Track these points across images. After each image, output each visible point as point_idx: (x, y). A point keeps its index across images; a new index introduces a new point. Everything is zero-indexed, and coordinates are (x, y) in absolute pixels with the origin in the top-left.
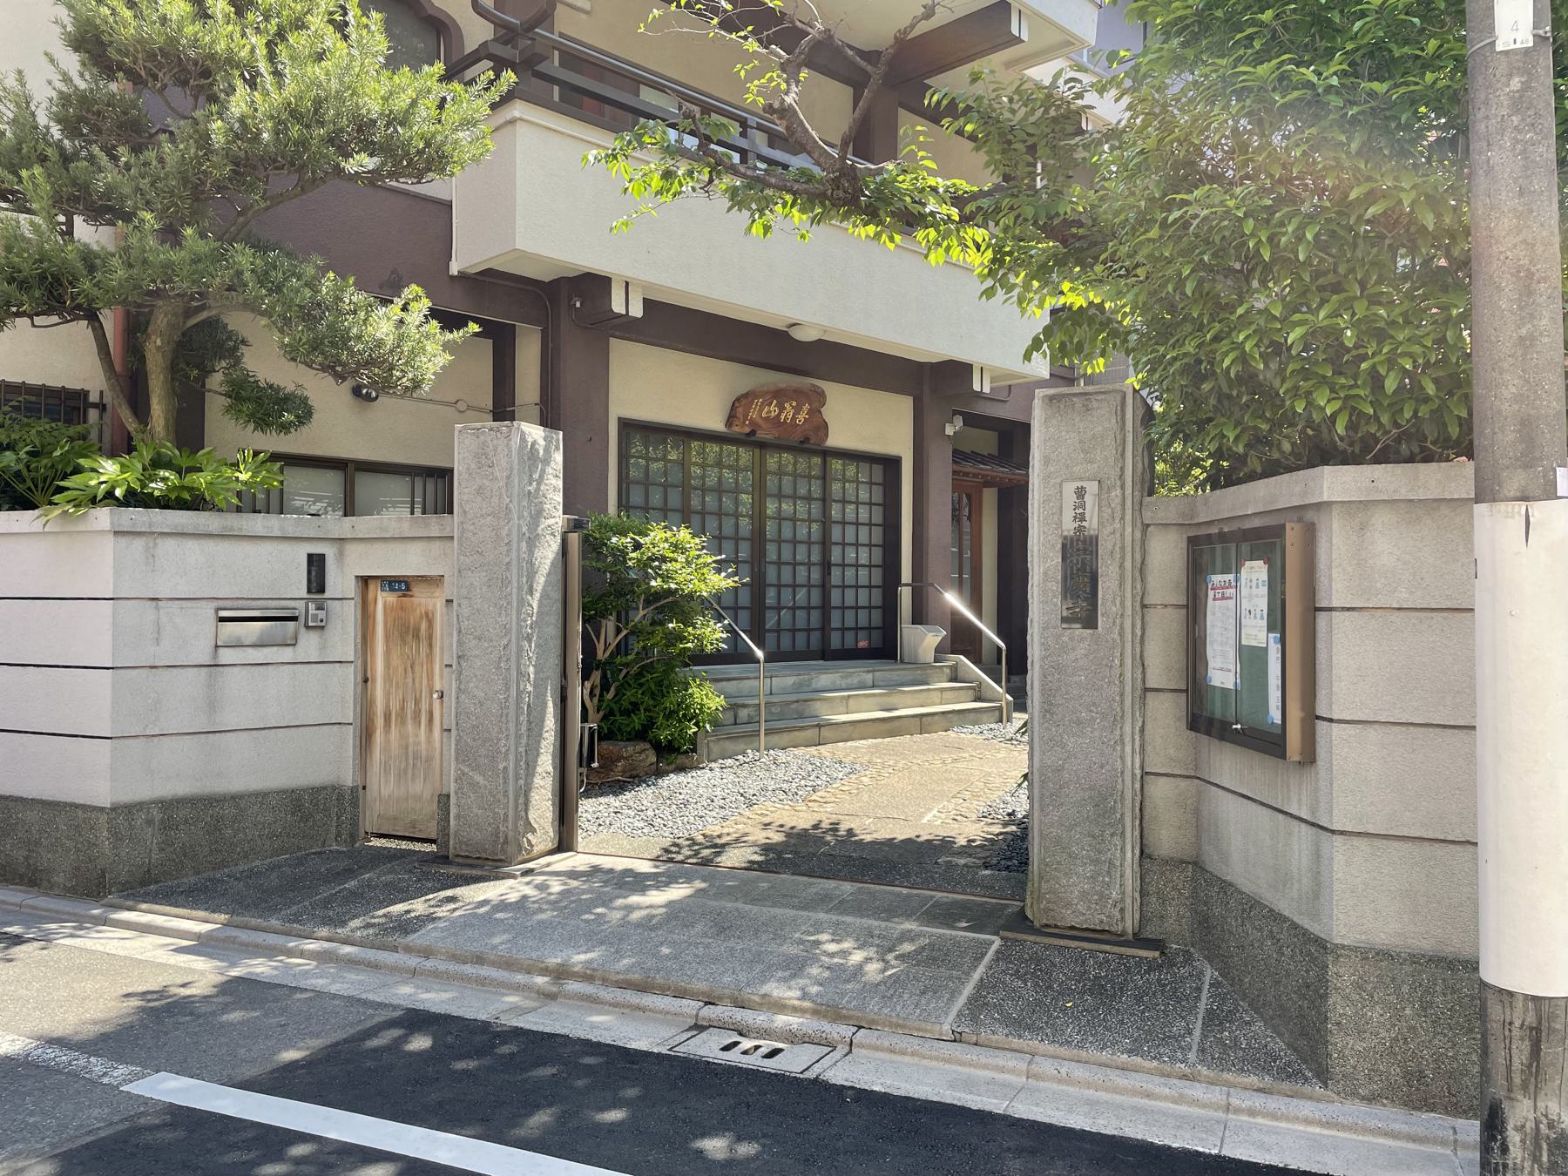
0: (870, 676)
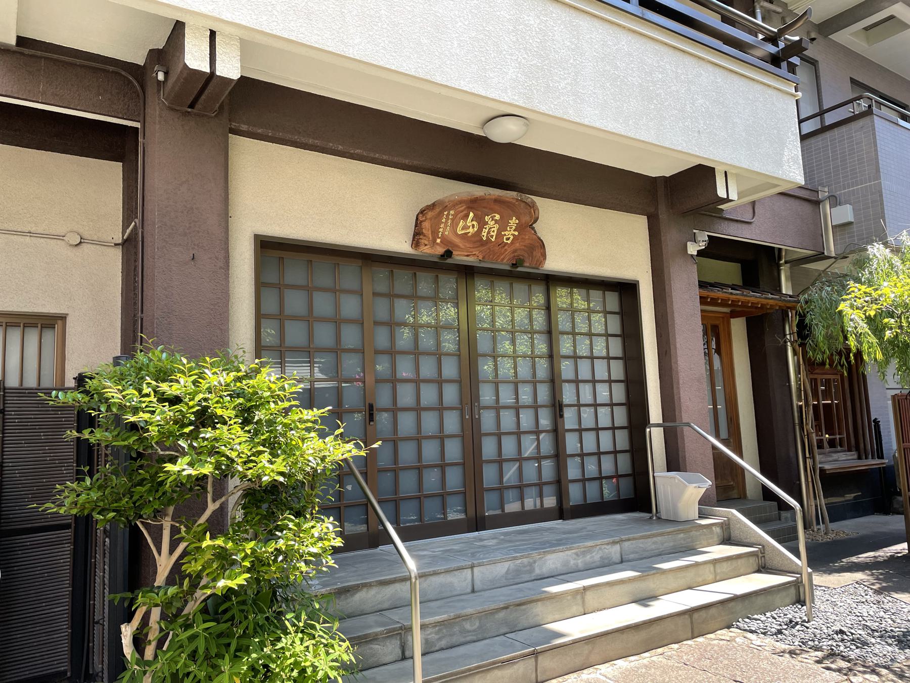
0: (617, 548)
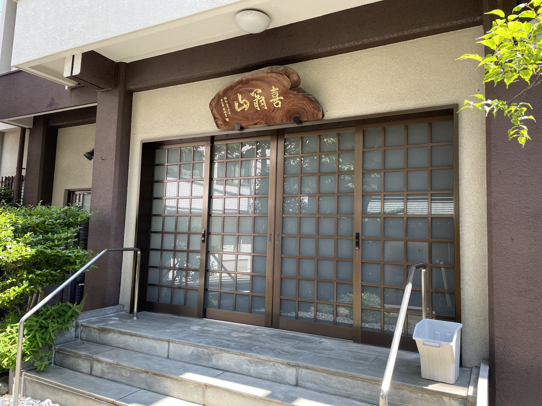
0: (293, 371)
